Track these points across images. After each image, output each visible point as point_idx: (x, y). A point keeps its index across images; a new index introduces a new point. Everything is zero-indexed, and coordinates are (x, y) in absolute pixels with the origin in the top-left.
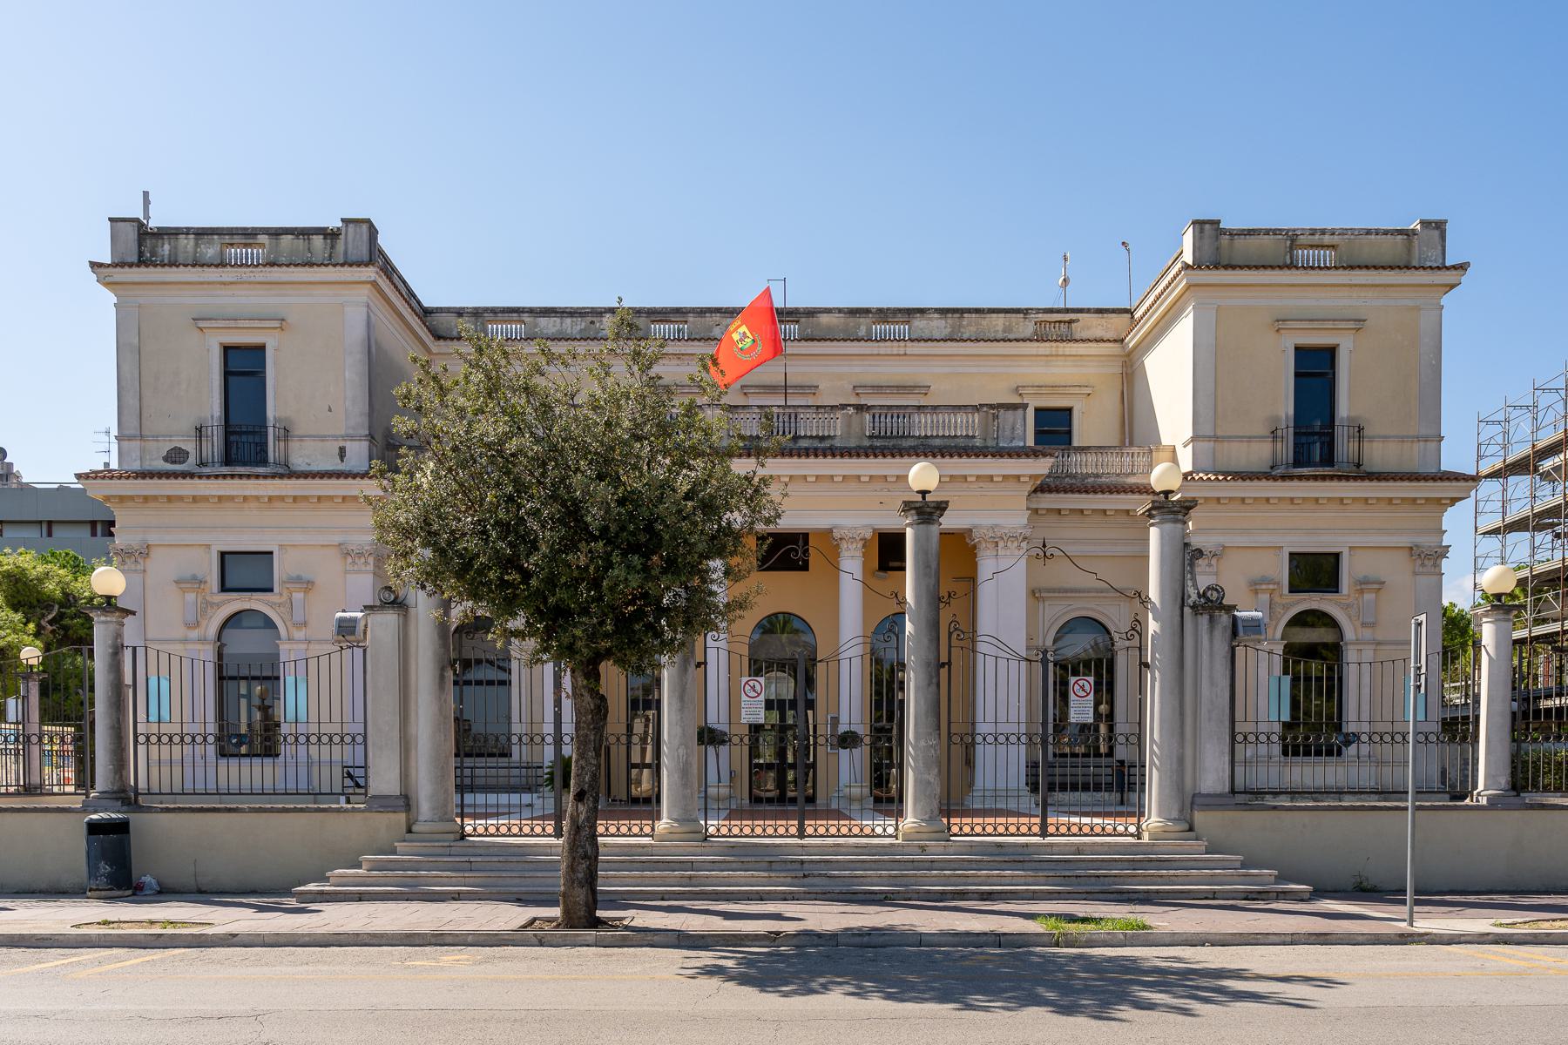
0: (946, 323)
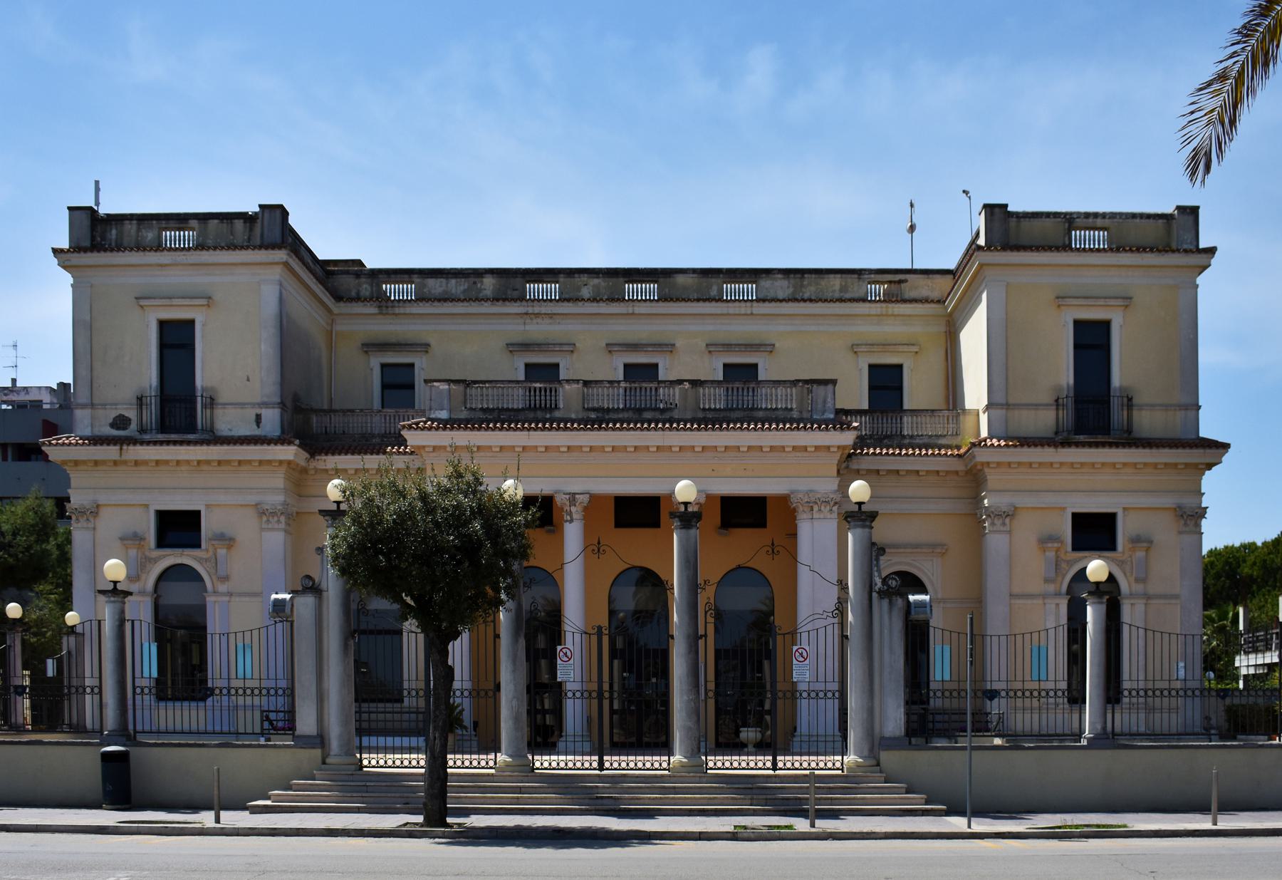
0: (789, 283)
